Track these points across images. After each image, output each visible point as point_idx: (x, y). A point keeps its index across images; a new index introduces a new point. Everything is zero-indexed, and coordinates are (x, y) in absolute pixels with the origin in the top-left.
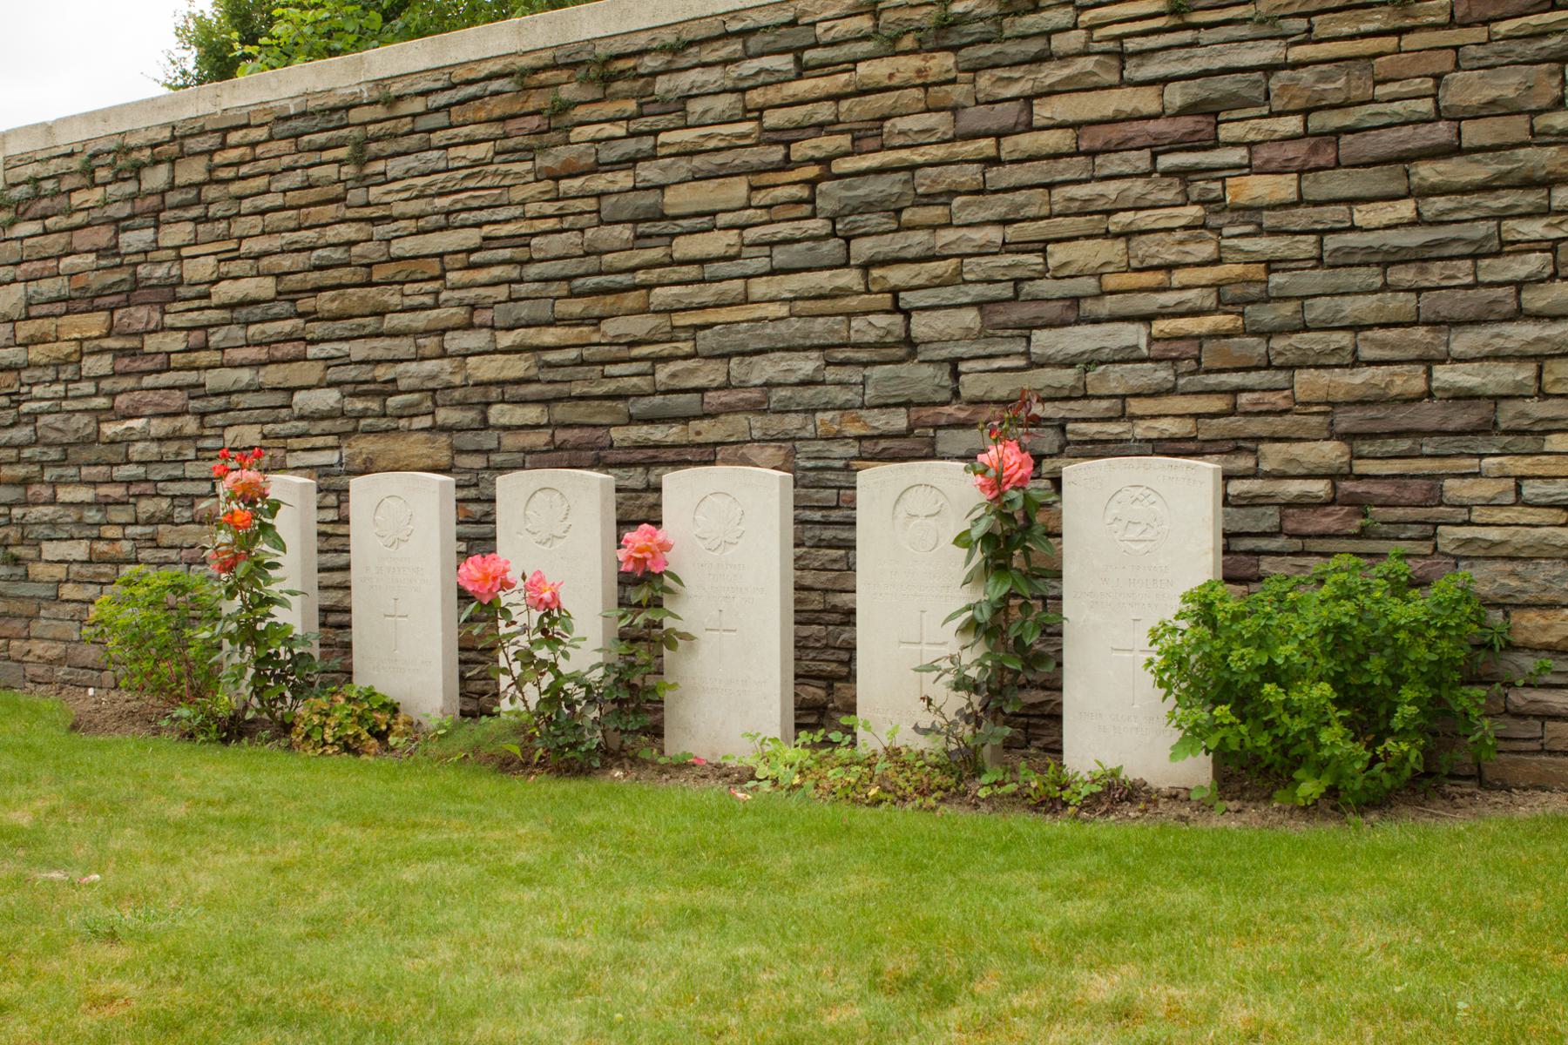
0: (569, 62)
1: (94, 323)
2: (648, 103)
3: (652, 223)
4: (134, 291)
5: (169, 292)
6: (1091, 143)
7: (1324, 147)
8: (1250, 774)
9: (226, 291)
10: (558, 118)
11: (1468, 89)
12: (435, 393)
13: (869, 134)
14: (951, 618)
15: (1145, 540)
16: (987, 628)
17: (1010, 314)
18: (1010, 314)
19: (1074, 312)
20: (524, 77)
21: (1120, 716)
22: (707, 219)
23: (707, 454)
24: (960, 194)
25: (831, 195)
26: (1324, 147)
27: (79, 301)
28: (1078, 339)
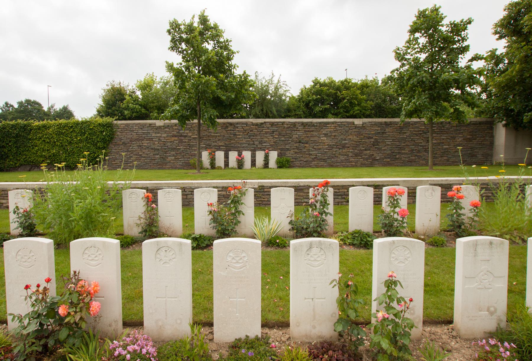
0: (228, 123)
1: (176, 138)
2: (235, 127)
3: (235, 135)
4: (181, 136)
5: (185, 136)
6: (266, 133)
7: (280, 134)
8: (280, 167)
9: (193, 137)
10: (227, 127)
11: (288, 132)
12: (215, 146)
13: (251, 131)
14: (79, 272)
15: (274, 155)
16: (265, 160)
17: (261, 143)
18: (261, 143)
19: (265, 143)
20: (224, 124)
21: (272, 163)
22: (239, 135)
23: (246, 150)
24: (385, 186)
25: (249, 134)
26: (280, 134)
27: (174, 136)
28: (265, 144)
